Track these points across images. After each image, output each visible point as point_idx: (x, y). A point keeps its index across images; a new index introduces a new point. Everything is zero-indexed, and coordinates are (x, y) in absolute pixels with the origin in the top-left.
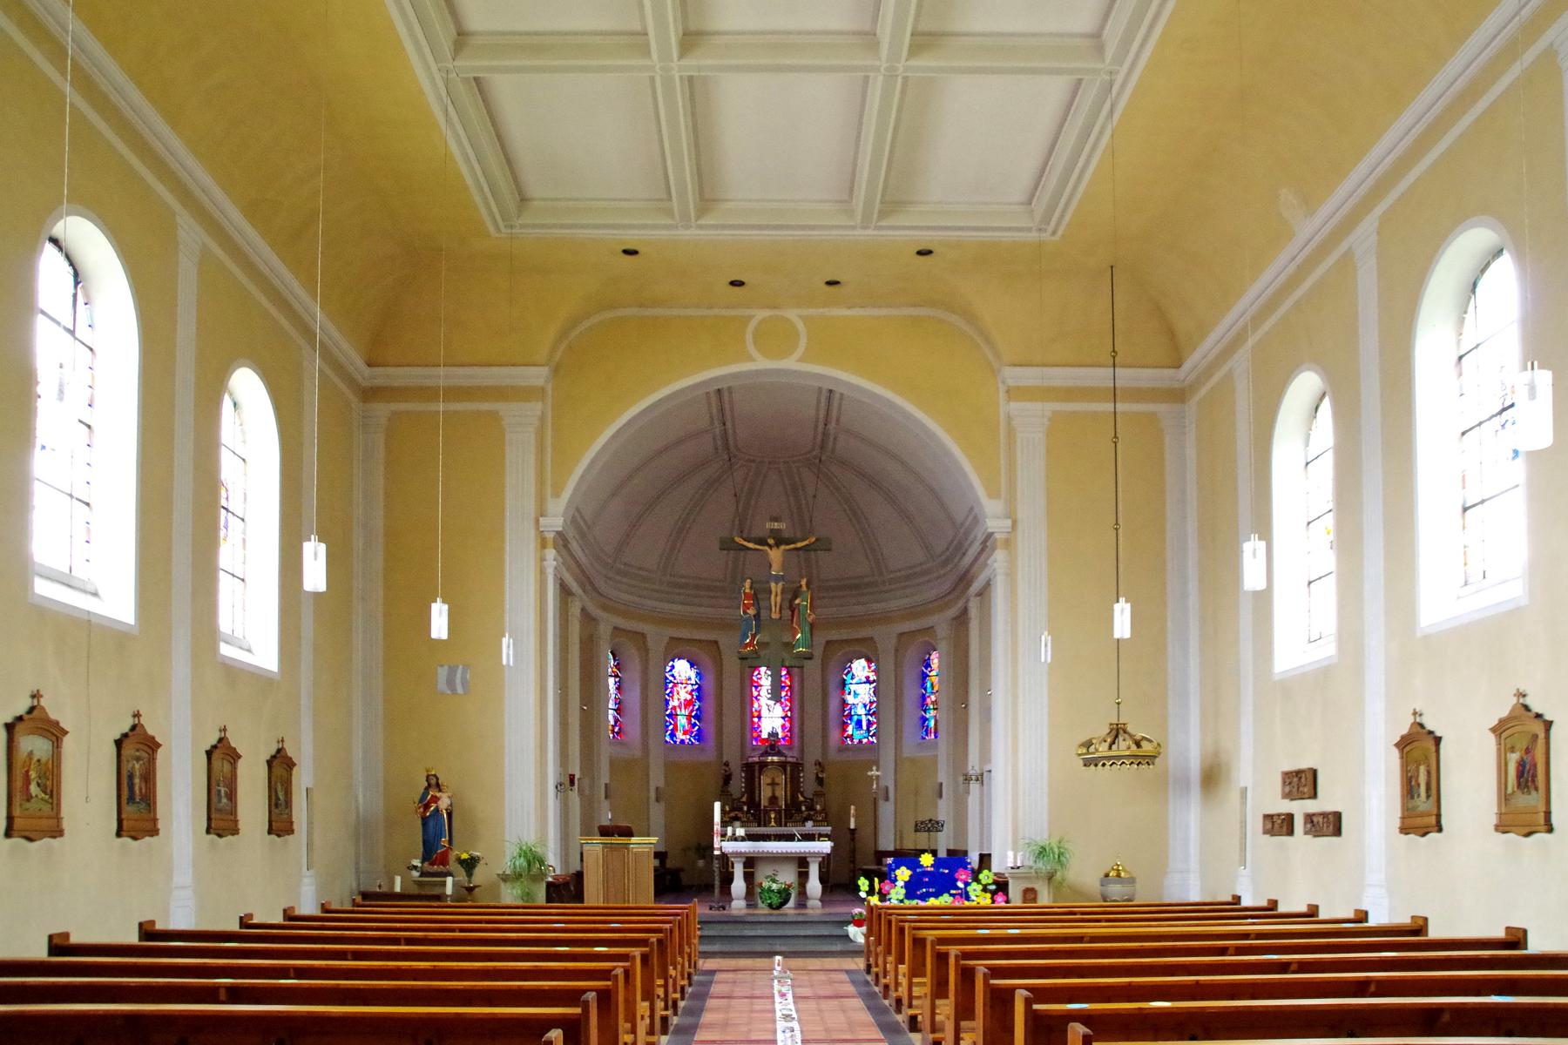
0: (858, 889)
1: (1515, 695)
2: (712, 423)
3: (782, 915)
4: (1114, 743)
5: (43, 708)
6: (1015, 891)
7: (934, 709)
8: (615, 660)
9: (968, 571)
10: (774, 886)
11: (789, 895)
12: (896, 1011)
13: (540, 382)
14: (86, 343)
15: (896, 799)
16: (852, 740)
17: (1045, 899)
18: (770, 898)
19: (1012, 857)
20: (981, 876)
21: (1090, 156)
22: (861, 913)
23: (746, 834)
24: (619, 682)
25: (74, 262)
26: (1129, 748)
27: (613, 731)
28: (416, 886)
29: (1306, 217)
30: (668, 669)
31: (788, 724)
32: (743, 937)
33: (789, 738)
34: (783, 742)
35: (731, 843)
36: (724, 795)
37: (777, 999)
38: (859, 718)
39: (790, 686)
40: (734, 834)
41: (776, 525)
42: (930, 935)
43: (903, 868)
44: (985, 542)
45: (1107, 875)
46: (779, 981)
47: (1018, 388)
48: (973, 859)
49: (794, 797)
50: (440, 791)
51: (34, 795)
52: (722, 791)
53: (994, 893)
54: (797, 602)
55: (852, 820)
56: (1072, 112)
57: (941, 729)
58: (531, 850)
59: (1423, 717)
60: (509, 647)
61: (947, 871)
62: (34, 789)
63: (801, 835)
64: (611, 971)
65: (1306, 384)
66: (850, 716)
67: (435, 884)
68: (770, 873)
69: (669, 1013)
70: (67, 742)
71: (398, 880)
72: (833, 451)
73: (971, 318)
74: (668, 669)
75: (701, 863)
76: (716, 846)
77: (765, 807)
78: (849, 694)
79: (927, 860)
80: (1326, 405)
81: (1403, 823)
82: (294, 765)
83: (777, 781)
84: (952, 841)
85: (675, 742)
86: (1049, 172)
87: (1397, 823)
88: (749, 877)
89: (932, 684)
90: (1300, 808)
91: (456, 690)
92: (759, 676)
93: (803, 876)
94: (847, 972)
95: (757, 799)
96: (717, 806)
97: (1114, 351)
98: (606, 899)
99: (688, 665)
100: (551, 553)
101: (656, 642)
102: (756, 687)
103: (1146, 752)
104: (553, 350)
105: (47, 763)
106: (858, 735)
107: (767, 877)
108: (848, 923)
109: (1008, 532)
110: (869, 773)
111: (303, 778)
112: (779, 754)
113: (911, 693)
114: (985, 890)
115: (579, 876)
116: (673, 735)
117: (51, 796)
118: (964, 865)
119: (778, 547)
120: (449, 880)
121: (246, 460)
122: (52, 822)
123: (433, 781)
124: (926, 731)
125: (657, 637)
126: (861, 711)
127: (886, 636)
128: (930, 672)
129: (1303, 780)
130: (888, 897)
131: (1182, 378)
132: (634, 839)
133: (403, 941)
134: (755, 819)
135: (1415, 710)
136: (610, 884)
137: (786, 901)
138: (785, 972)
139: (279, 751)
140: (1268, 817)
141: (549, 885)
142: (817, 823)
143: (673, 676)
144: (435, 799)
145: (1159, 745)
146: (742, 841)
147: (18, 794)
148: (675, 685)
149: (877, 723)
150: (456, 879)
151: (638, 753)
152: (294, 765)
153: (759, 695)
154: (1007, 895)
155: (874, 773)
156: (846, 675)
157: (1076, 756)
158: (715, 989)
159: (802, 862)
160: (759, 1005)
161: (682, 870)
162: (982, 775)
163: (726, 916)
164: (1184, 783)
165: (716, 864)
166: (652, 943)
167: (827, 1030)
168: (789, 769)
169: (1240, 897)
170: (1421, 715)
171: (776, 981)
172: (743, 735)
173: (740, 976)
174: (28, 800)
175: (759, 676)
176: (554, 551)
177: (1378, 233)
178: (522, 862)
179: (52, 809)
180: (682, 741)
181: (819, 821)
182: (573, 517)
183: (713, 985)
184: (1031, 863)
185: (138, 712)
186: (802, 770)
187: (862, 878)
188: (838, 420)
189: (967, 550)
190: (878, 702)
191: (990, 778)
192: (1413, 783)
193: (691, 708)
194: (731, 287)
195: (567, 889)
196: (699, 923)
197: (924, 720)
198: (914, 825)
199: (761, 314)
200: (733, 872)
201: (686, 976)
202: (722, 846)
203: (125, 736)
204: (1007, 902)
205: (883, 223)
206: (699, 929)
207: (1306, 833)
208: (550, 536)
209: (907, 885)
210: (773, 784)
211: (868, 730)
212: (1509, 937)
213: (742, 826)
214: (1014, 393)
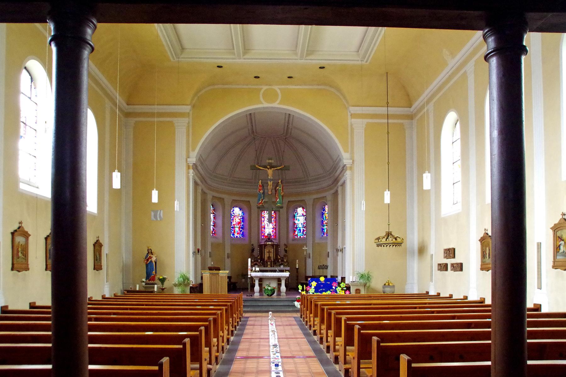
0: (298, 289)
1: (561, 215)
2: (248, 124)
3: (272, 298)
4: (387, 238)
5: (23, 227)
6: (353, 290)
7: (326, 226)
8: (213, 208)
9: (337, 177)
10: (269, 288)
12: (309, 329)
13: (188, 111)
14: (24, 95)
15: (313, 258)
16: (297, 236)
17: (363, 292)
18: (268, 292)
19: (352, 278)
20: (341, 285)
21: (378, 38)
22: (299, 298)
24: (214, 215)
25: (31, 75)
26: (392, 240)
27: (212, 233)
28: (144, 288)
29: (452, 59)
30: (232, 211)
31: (274, 231)
32: (259, 306)
33: (275, 236)
34: (273, 237)
35: (254, 273)
36: (252, 256)
37: (270, 325)
38: (300, 228)
39: (275, 217)
41: (270, 161)
42: (319, 303)
43: (314, 282)
44: (343, 167)
45: (385, 285)
46: (271, 320)
47: (355, 114)
48: (339, 279)
50: (152, 255)
51: (20, 256)
52: (251, 255)
53: (345, 291)
54: (277, 188)
55: (297, 265)
56: (363, 42)
57: (329, 234)
58: (185, 275)
59: (488, 231)
60: (177, 204)
61: (329, 283)
62: (20, 254)
64: (208, 319)
65: (452, 116)
66: (297, 228)
67: (149, 287)
69: (230, 336)
70: (30, 239)
71: (138, 286)
72: (291, 133)
73: (339, 90)
74: (232, 211)
75: (243, 280)
78: (296, 220)
79: (322, 279)
80: (458, 124)
81: (481, 267)
82: (102, 246)
84: (332, 273)
85: (234, 237)
86: (364, 42)
87: (480, 267)
88: (260, 285)
89: (326, 217)
90: (449, 261)
91: (157, 219)
93: (279, 285)
94: (294, 317)
95: (263, 257)
96: (249, 260)
97: (387, 102)
98: (211, 292)
99: (239, 209)
100: (191, 171)
101: (228, 199)
102: (263, 217)
103: (398, 241)
104: (192, 100)
105: (24, 245)
106: (299, 235)
107: (267, 285)
108: (294, 301)
109: (352, 164)
110: (303, 248)
111: (105, 250)
112: (271, 241)
113: (318, 220)
114: (342, 289)
115: (201, 285)
116: (233, 234)
117: (25, 257)
118: (335, 281)
119: (271, 169)
120: (156, 286)
121: (37, 104)
122: (26, 265)
123: (150, 251)
124: (324, 233)
125: (228, 199)
126: (300, 226)
127: (309, 199)
128: (325, 212)
129: (451, 252)
130: (309, 292)
131: (412, 111)
132: (220, 272)
133: (129, 309)
134: (263, 264)
135: (485, 228)
136: (212, 287)
137: (273, 293)
138: (273, 317)
139: (97, 241)
140: (439, 265)
141: (191, 288)
142: (284, 266)
143: (233, 213)
144: (151, 258)
145: (403, 239)
146: (258, 272)
147: (16, 256)
148: (235, 216)
149: (306, 230)
150: (158, 286)
152: (102, 246)
153: (264, 220)
154: (350, 291)
155: (305, 248)
156: (295, 213)
157: (374, 243)
158: (248, 323)
159: (279, 280)
160: (263, 328)
161: (237, 283)
162: (343, 249)
163: (253, 298)
164: (413, 253)
165: (249, 281)
166: (218, 314)
167: (286, 335)
169: (428, 292)
170: (487, 230)
171: (269, 320)
172: (258, 238)
173: (257, 319)
174: (18, 258)
175: (264, 213)
176: (192, 170)
177: (474, 66)
178: (181, 279)
179: (26, 261)
180: (237, 236)
182: (199, 157)
183: (248, 321)
184: (358, 280)
185: (21, 221)
186: (280, 247)
187: (300, 285)
188: (292, 123)
189: (337, 170)
190: (306, 223)
191: (345, 250)
192: (485, 253)
194: (255, 78)
195: (198, 289)
196: (243, 301)
197: (323, 229)
198: (318, 267)
199: (265, 88)
200: (255, 284)
201: (239, 318)
202: (251, 274)
203: (16, 231)
204: (350, 293)
205: (307, 58)
206: (243, 303)
207: (451, 270)
208: (191, 165)
209: (315, 288)
210: (269, 252)
211: (303, 233)
212: (535, 307)
213: (258, 267)
214: (353, 116)
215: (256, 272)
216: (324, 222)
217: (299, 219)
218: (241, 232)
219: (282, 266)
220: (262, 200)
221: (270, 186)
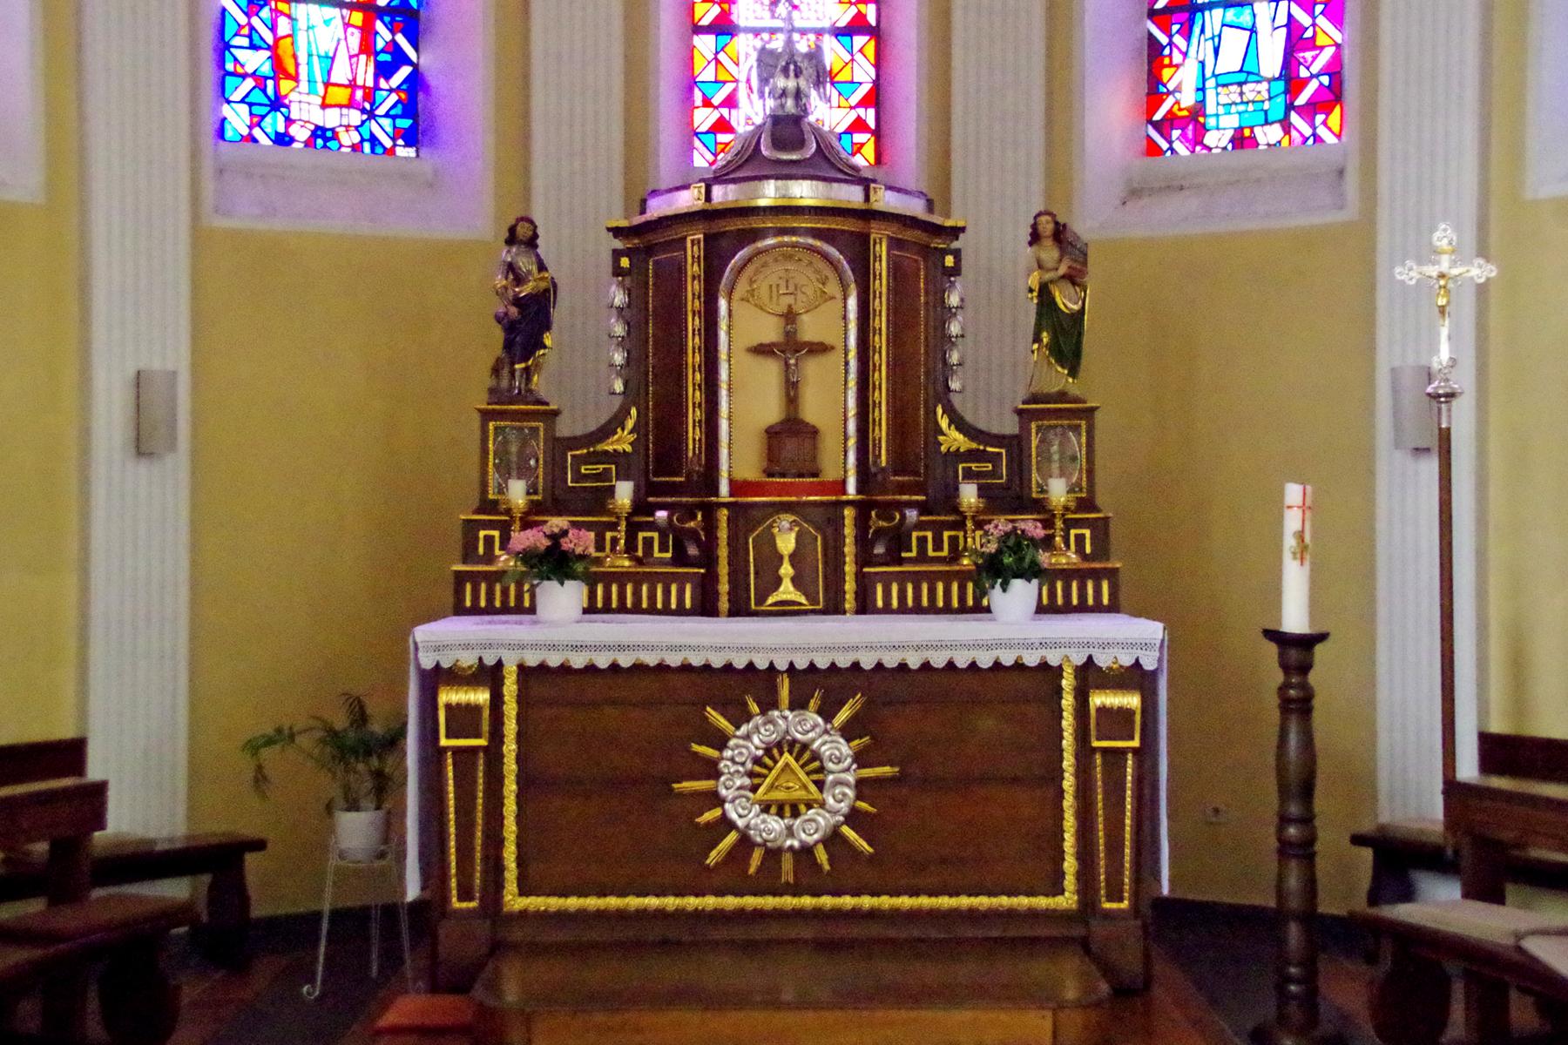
16: (1197, 140)
55: (1295, 585)
77: (737, 487)
95: (694, 434)
134: (680, 558)
161: (259, 845)
218: (384, 71)
219: (1017, 584)
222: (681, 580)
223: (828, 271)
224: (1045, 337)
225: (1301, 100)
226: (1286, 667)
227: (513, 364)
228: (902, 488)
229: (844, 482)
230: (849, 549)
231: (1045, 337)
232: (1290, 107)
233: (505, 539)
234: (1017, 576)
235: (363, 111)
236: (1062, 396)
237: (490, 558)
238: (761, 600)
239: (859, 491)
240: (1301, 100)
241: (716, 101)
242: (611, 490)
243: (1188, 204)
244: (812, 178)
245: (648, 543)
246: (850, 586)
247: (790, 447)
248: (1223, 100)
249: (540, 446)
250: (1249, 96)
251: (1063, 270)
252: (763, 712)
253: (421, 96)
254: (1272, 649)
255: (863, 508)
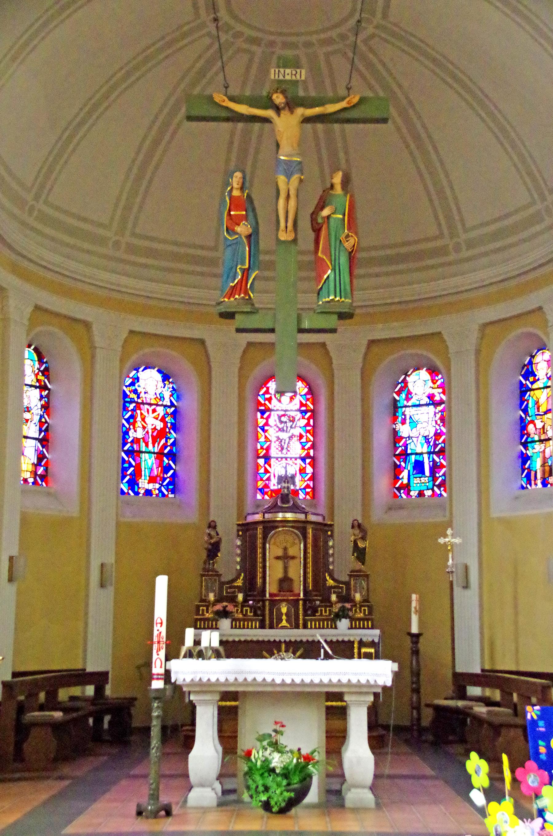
11: (306, 780)
16: (408, 494)
23: (221, 642)
24: (47, 396)
30: (128, 381)
31: (309, 470)
38: (419, 458)
40: (197, 642)
41: (288, 74)
49: (319, 581)
54: (326, 212)
55: (415, 619)
63: (330, 643)
66: (405, 455)
68: (268, 729)
76: (157, 669)
77: (271, 595)
83: (291, 552)
89: (537, 403)
92: (267, 396)
95: (259, 581)
99: (159, 377)
102: (263, 413)
110: (441, 541)
112: (295, 508)
119: (292, 111)
124: (528, 476)
128: (532, 383)
134: (255, 614)
137: (302, 793)
143: (135, 391)
148: (138, 406)
151: (74, 510)
153: (267, 424)
156: (399, 393)
168: (310, 531)
175: (267, 396)
180: (148, 493)
181: (360, 619)
186: (332, 536)
187: (474, 755)
193: (163, 441)
197: (525, 458)
210: (286, 558)
215: (201, 655)
216: (531, 427)
217: (415, 418)
219: (343, 620)
220: (244, 271)
221: (288, 197)
222: (256, 620)
223: (295, 537)
224: (355, 555)
225: (437, 483)
226: (413, 642)
227: (209, 561)
228: (316, 596)
229: (300, 594)
230: (301, 611)
231: (355, 555)
232: (434, 485)
233: (207, 610)
234: (343, 618)
235: (160, 484)
236: (360, 571)
237: (203, 614)
238: (277, 625)
239: (304, 596)
240: (437, 483)
241: (264, 479)
242: (237, 596)
243: (404, 513)
244: (292, 512)
245: (246, 611)
246: (301, 622)
247: (285, 586)
248: (415, 482)
249: (217, 584)
250: (423, 481)
251: (360, 536)
252: (278, 653)
253: (176, 479)
254: (409, 638)
255: (305, 601)
